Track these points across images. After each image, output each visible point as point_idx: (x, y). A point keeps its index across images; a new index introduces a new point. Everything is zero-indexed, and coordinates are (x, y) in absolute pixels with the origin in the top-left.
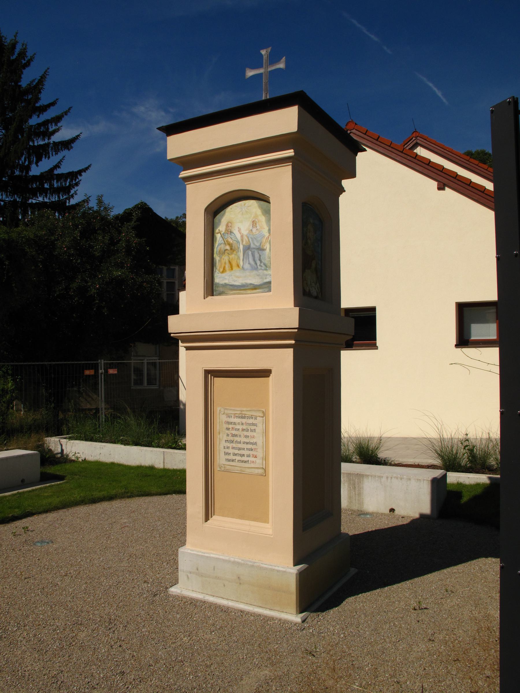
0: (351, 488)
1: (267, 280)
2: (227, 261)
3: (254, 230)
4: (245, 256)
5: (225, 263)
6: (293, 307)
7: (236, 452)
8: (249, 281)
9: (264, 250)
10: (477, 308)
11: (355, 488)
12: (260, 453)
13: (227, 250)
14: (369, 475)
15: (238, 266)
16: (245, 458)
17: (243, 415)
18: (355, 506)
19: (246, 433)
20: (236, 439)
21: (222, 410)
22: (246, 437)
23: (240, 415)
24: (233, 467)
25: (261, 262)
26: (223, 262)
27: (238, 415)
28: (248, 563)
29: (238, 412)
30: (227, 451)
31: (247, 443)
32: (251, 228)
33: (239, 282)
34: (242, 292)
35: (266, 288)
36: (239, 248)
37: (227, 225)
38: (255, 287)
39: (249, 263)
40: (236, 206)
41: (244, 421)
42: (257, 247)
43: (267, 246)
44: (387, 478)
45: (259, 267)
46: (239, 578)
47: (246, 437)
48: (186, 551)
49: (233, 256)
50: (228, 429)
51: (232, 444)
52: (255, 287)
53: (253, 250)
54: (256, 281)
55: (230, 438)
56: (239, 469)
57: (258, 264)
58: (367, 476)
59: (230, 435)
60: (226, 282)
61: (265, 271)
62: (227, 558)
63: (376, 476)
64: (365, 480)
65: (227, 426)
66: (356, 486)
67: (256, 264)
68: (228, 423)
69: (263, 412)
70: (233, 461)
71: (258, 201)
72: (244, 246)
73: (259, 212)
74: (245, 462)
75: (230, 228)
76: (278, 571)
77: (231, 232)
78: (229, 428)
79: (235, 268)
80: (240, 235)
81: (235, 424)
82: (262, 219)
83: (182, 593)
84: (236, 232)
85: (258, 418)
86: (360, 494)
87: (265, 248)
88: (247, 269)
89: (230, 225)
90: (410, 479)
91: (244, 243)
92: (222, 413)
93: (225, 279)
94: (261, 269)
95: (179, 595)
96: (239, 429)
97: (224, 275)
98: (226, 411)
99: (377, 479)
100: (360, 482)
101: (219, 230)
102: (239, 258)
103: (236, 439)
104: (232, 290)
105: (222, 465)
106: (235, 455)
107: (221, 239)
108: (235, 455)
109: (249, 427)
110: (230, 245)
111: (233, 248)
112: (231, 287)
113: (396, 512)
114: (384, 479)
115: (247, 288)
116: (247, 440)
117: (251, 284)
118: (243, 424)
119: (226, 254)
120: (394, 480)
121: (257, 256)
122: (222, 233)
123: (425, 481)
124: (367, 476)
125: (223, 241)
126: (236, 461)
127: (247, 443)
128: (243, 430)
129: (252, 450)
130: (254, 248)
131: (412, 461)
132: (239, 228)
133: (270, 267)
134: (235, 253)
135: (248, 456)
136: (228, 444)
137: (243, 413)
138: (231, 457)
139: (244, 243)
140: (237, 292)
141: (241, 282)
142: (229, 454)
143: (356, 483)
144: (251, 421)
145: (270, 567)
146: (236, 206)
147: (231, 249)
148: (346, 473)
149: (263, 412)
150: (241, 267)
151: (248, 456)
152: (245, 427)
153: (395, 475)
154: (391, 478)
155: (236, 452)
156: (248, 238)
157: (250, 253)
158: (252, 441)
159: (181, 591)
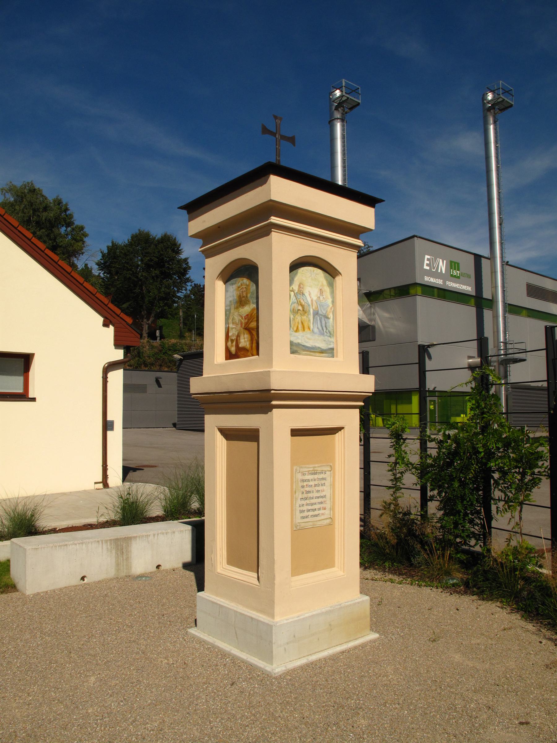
0: (119, 554)
1: (331, 346)
2: (300, 321)
3: (321, 298)
4: (315, 320)
5: (298, 323)
6: (358, 373)
7: (310, 507)
8: (318, 345)
9: (328, 318)
10: (8, 359)
11: (123, 553)
12: (328, 506)
13: (299, 310)
14: (137, 537)
15: (309, 328)
16: (316, 513)
17: (315, 472)
18: (123, 572)
19: (317, 488)
20: (310, 495)
21: (298, 468)
22: (318, 491)
23: (313, 472)
24: (306, 524)
25: (326, 328)
26: (297, 321)
27: (311, 472)
28: (337, 607)
29: (311, 469)
30: (302, 508)
31: (318, 497)
32: (319, 295)
33: (309, 344)
34: (312, 353)
35: (329, 353)
36: (309, 311)
37: (299, 286)
38: (322, 351)
39: (318, 328)
40: (307, 270)
41: (316, 476)
42: (323, 315)
43: (331, 316)
44: (154, 535)
45: (325, 333)
46: (330, 625)
47: (318, 491)
48: (282, 623)
49: (305, 317)
50: (303, 487)
51: (306, 501)
52: (322, 351)
53: (320, 316)
54: (323, 346)
55: (305, 495)
56: (311, 523)
57: (325, 330)
58: (135, 537)
59: (305, 493)
60: (299, 341)
61: (329, 338)
62: (319, 611)
63: (143, 536)
64: (133, 542)
65: (302, 484)
66: (124, 551)
67: (323, 329)
68: (303, 481)
69: (331, 466)
70: (307, 517)
71: (324, 272)
72: (313, 310)
73: (325, 283)
74: (316, 516)
75: (302, 289)
76: (358, 603)
77: (303, 294)
78: (304, 486)
79: (306, 330)
80: (310, 300)
81: (309, 481)
82: (327, 289)
83: (288, 668)
84: (307, 295)
85: (327, 472)
86: (128, 559)
87: (329, 317)
88: (316, 334)
89: (302, 286)
90: (174, 532)
91: (314, 307)
92: (298, 471)
93: (298, 338)
94: (327, 336)
95: (285, 672)
96: (312, 485)
97: (297, 334)
98: (301, 470)
99: (144, 538)
100: (128, 546)
101: (292, 288)
102: (309, 320)
103: (310, 495)
104: (304, 350)
105: (298, 524)
106: (308, 511)
107: (294, 298)
108: (308, 511)
109: (320, 482)
110: (303, 306)
111: (305, 310)
112: (304, 348)
113: (162, 568)
114: (151, 538)
115: (316, 351)
116: (318, 495)
117: (319, 348)
118: (315, 480)
119: (299, 314)
120: (161, 536)
121: (323, 322)
122: (295, 292)
123: (187, 531)
124: (135, 537)
125: (296, 301)
126: (310, 516)
127: (318, 497)
128: (315, 485)
129: (322, 503)
130: (321, 315)
131: (65, 524)
132: (309, 291)
133: (333, 336)
134: (306, 315)
135: (319, 509)
136: (304, 502)
137: (315, 469)
138: (306, 514)
139: (314, 307)
140: (308, 353)
141: (312, 344)
142: (304, 511)
143: (124, 548)
144: (321, 476)
145: (352, 602)
146: (307, 270)
147: (303, 310)
148: (114, 539)
149: (331, 466)
150: (311, 330)
151: (319, 509)
152: (316, 483)
153: (160, 531)
154: (158, 534)
155: (310, 507)
156: (317, 303)
157: (318, 318)
158: (322, 495)
159: (286, 667)
